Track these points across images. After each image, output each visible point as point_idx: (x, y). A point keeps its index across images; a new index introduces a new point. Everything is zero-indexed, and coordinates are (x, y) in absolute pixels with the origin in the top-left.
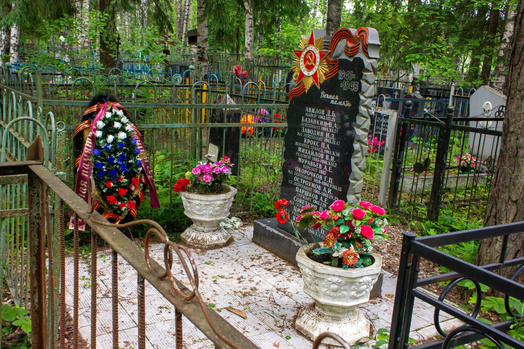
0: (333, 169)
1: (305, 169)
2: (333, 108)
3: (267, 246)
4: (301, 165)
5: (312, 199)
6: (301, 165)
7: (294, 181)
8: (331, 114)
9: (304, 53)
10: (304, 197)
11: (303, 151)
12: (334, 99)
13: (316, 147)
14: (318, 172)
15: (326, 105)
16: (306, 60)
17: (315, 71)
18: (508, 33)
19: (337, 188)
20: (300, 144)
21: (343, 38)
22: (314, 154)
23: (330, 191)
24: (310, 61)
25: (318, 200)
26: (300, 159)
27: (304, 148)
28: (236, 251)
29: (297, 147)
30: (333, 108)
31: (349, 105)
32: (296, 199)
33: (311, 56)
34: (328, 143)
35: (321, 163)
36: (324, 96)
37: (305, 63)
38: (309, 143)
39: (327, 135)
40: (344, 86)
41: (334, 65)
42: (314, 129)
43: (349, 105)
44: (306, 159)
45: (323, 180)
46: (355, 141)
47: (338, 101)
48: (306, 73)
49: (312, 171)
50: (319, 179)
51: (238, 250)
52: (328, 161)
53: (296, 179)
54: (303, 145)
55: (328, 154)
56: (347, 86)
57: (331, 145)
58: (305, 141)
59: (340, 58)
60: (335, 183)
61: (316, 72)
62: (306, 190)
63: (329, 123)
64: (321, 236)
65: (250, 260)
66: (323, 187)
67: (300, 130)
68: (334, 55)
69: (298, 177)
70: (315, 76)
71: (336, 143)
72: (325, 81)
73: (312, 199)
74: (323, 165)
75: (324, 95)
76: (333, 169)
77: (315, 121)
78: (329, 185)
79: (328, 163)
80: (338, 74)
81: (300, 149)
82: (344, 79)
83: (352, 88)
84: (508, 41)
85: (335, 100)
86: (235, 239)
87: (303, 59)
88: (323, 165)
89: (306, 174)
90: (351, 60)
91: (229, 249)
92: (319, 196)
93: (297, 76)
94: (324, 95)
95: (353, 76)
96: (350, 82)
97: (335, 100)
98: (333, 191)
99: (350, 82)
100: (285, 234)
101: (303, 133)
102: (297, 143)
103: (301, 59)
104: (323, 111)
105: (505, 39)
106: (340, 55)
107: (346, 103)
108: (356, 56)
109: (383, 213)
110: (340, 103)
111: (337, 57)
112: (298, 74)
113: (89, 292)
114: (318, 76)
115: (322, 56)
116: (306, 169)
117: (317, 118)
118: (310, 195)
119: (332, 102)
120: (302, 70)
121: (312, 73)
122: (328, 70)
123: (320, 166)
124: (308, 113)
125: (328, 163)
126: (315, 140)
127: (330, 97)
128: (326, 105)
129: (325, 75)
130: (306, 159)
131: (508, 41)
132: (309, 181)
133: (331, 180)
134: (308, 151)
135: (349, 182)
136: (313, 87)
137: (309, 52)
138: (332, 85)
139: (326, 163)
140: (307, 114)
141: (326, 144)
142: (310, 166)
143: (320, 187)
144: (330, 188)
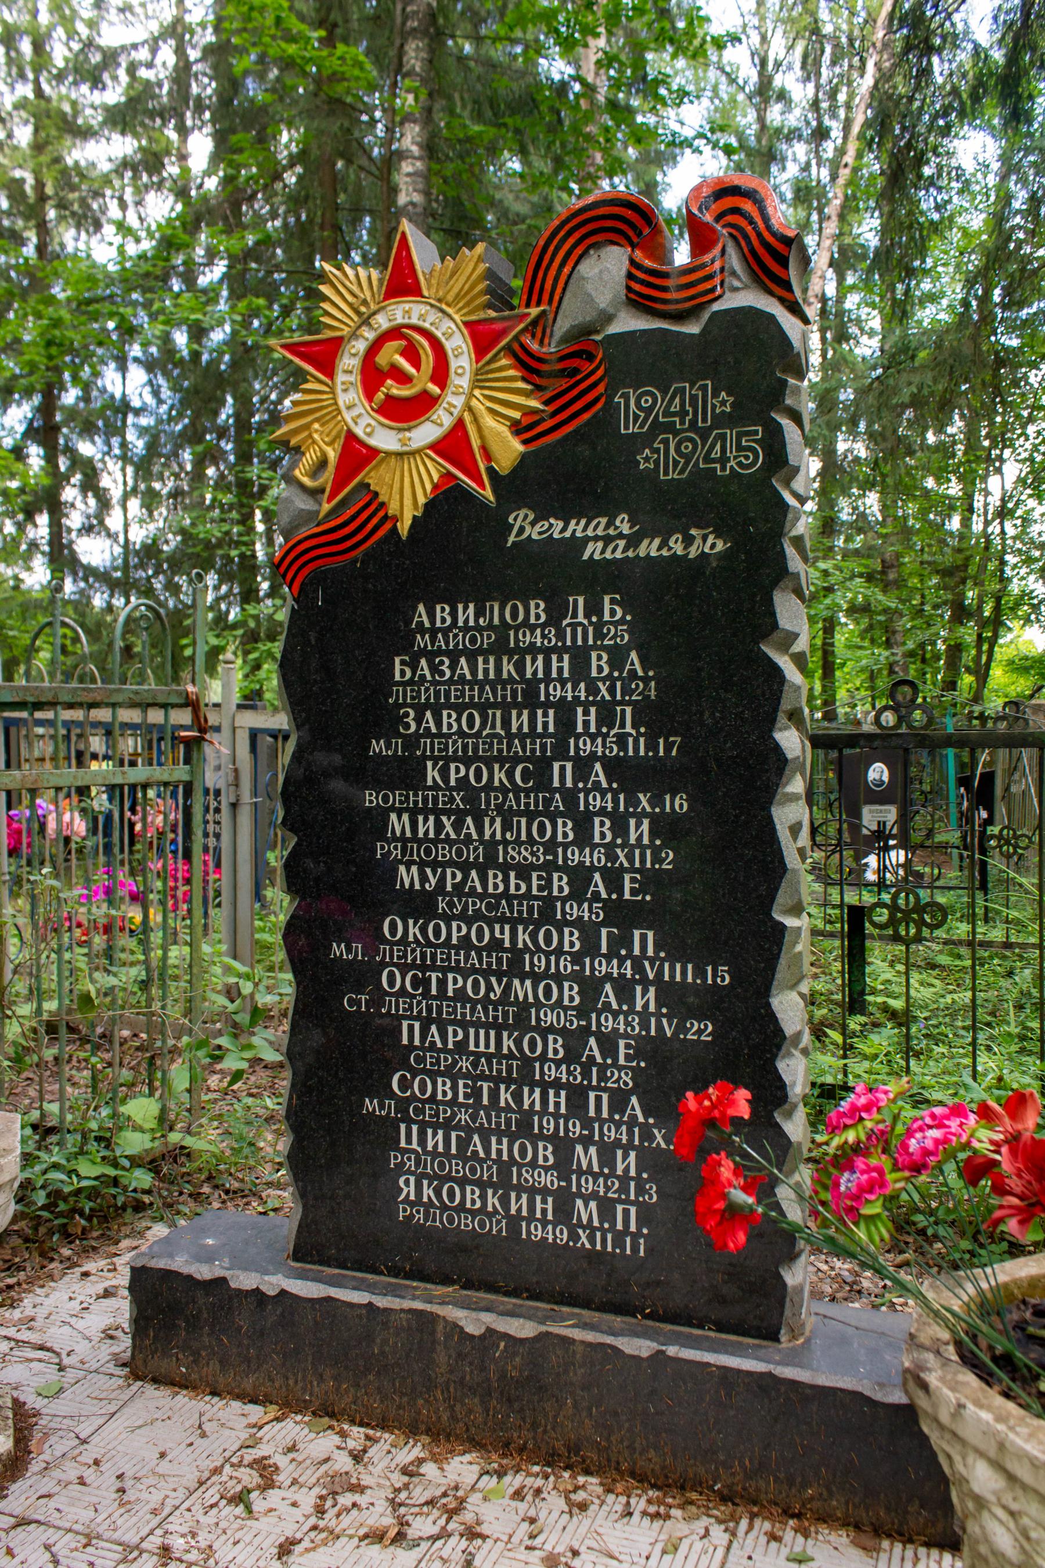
0: (650, 880)
1: (448, 919)
3: (248, 1384)
4: (420, 905)
5: (527, 1063)
6: (420, 905)
7: (378, 997)
8: (593, 608)
9: (360, 346)
10: (465, 1064)
11: (426, 827)
12: (602, 538)
13: (517, 790)
14: (547, 915)
15: (557, 575)
16: (372, 376)
17: (448, 422)
19: (699, 972)
20: (395, 798)
21: (597, 246)
22: (506, 827)
23: (646, 998)
24: (403, 379)
25: (572, 1056)
26: (407, 877)
27: (426, 812)
28: (104, 1484)
29: (383, 814)
32: (404, 1084)
33: (411, 354)
34: (593, 757)
35: (565, 869)
36: (534, 533)
37: (370, 395)
38: (463, 782)
39: (585, 719)
40: (666, 461)
41: (576, 371)
42: (483, 708)
44: (451, 863)
45: (590, 947)
46: (782, 719)
47: (633, 541)
48: (385, 439)
49: (503, 920)
50: (559, 952)
51: (109, 1470)
52: (610, 848)
53: (394, 980)
54: (416, 798)
55: (602, 812)
56: (688, 458)
57: (612, 766)
58: (432, 774)
59: (614, 329)
60: (674, 947)
61: (460, 424)
62: (477, 1025)
63: (589, 663)
64: (592, 1239)
65: (229, 1511)
66: (591, 988)
67: (388, 722)
68: (562, 326)
69: (404, 969)
70: (454, 445)
71: (652, 746)
72: (524, 457)
73: (527, 1063)
74: (580, 877)
75: (526, 526)
76: (650, 880)
77: (486, 667)
78: (638, 967)
79: (612, 857)
80: (611, 409)
81: (399, 824)
82: (657, 428)
83: (723, 460)
85: (607, 540)
86: (32, 1401)
87: (355, 378)
88: (580, 877)
89: (465, 942)
90: (693, 329)
91: (47, 1485)
92: (575, 1041)
93: (323, 463)
94: (526, 526)
95: (724, 402)
96: (704, 434)
97: (607, 540)
98: (668, 993)
99: (704, 434)
100: (370, 1288)
101: (411, 742)
102: (371, 799)
103: (340, 378)
104: (538, 610)
106: (608, 318)
107: (688, 541)
108: (716, 307)
110: (649, 548)
111: (585, 331)
112: (332, 455)
114: (475, 443)
115: (482, 339)
116: (463, 917)
117: (500, 648)
118: (508, 1043)
119: (593, 551)
120: (359, 431)
121: (427, 432)
122: (534, 404)
123: (561, 884)
124: (433, 632)
125: (612, 857)
126: (501, 760)
127: (577, 528)
128: (557, 575)
129: (517, 429)
130: (451, 863)
132: (487, 973)
133: (644, 940)
134: (458, 826)
135: (783, 927)
136: (447, 500)
137: (394, 333)
138: (571, 465)
139: (599, 858)
140: (421, 641)
141: (583, 766)
142: (482, 897)
143: (571, 993)
144: (645, 983)
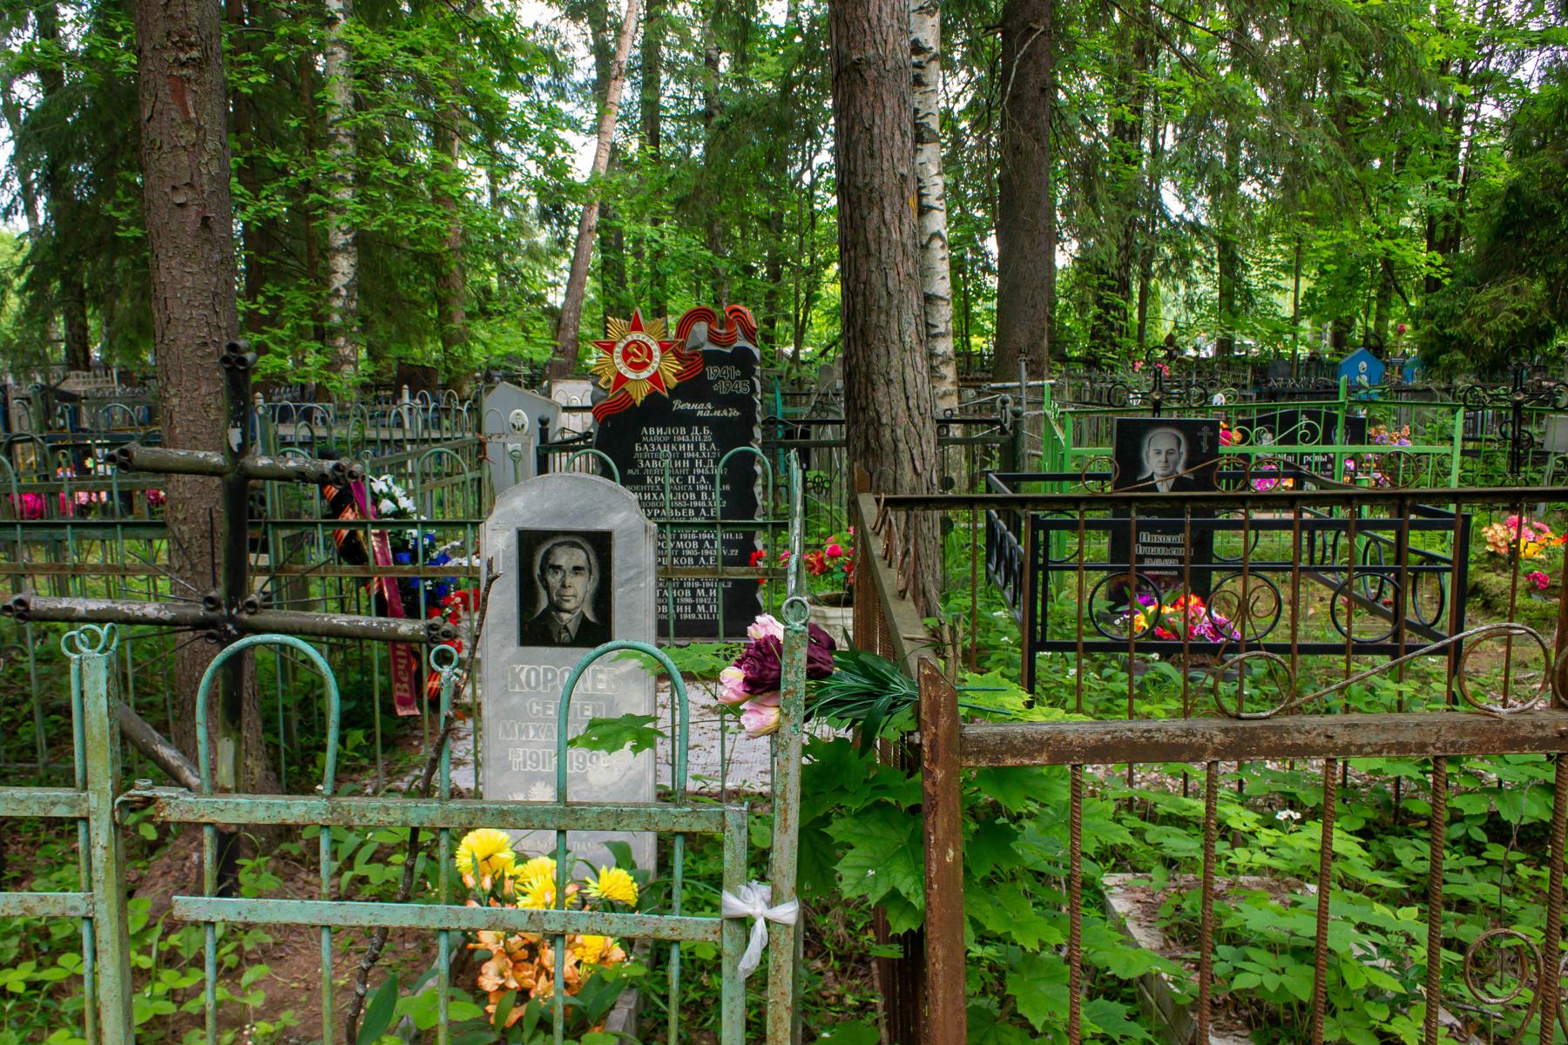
2: (702, 422)
12: (703, 410)
18: (339, 275)
30: (702, 422)
31: (736, 413)
40: (722, 388)
43: (736, 413)
58: (649, 480)
75: (679, 405)
84: (344, 292)
90: (728, 351)
94: (679, 405)
101: (642, 470)
104: (683, 430)
105: (338, 290)
109: (1307, 374)
110: (717, 413)
113: (1066, 484)
119: (700, 413)
127: (695, 406)
128: (689, 420)
131: (344, 292)
141: (698, 477)
